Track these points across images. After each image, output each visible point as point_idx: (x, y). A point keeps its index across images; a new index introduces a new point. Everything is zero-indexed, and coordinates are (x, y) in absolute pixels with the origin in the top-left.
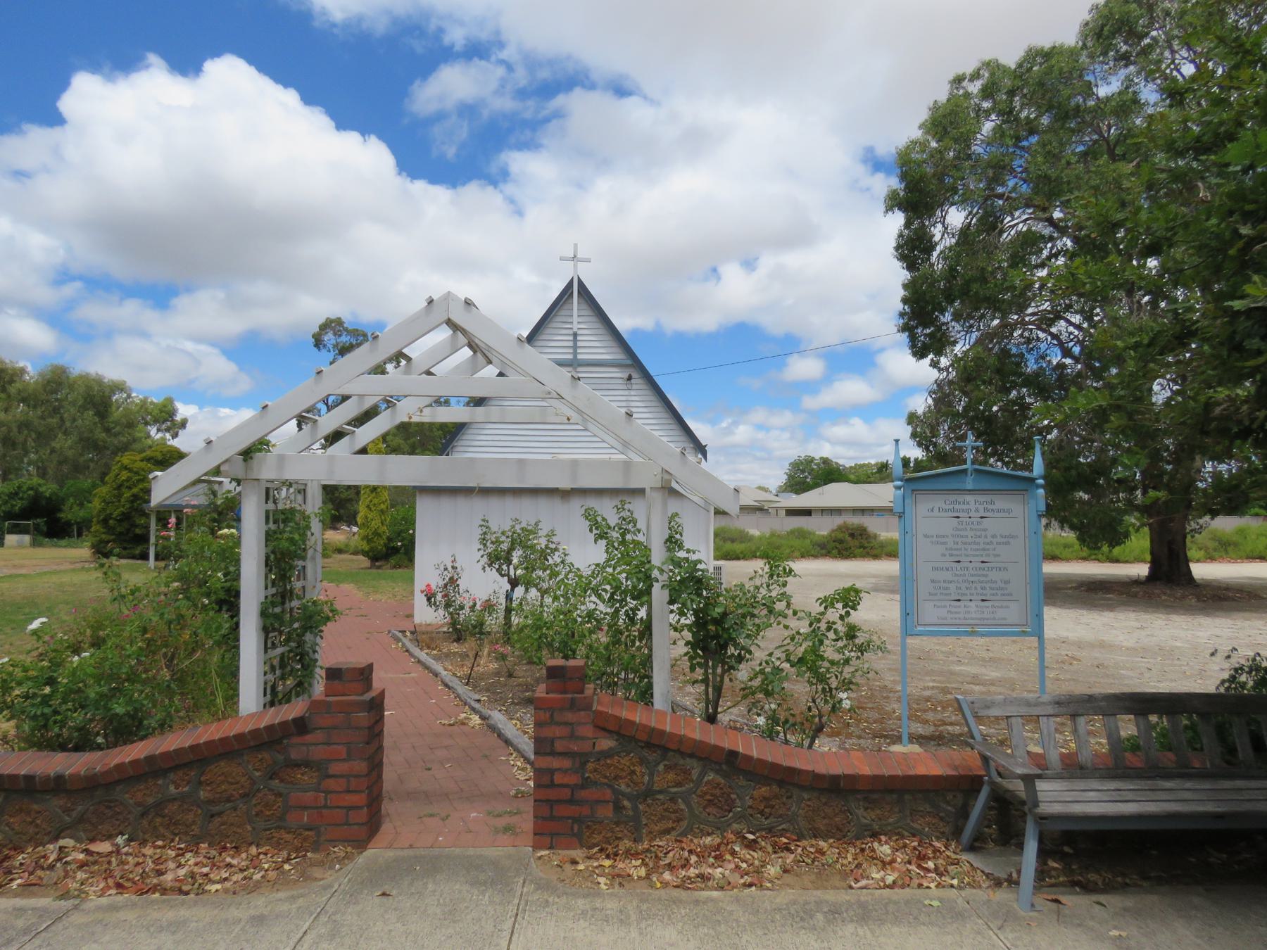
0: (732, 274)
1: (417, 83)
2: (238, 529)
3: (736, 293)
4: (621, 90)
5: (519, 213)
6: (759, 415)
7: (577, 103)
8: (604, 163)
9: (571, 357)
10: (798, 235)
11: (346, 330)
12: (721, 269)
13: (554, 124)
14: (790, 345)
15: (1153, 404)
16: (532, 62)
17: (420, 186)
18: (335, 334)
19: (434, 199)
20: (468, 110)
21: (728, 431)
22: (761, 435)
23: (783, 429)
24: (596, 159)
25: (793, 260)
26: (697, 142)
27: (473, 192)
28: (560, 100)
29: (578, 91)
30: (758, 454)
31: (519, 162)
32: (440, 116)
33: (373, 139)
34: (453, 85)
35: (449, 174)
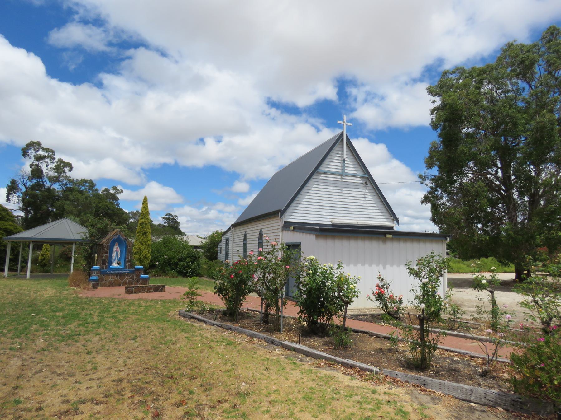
0: (210, 142)
1: (56, 29)
2: (20, 242)
3: (211, 151)
4: (163, 54)
5: (109, 102)
6: (220, 206)
7: (141, 55)
8: (151, 84)
9: (340, 171)
10: (241, 129)
11: (42, 148)
12: (205, 140)
13: (126, 62)
14: (235, 176)
15: (91, 235)
16: (119, 32)
17: (54, 82)
18: (35, 150)
19: (65, 90)
20: (78, 49)
21: (206, 212)
22: (221, 215)
23: (230, 213)
24: (147, 82)
25: (238, 140)
26: (198, 83)
27: (85, 88)
28: (131, 52)
29: (142, 50)
30: (219, 223)
31: (108, 79)
32: (65, 49)
33: (32, 54)
34: (73, 34)
35: (75, 77)
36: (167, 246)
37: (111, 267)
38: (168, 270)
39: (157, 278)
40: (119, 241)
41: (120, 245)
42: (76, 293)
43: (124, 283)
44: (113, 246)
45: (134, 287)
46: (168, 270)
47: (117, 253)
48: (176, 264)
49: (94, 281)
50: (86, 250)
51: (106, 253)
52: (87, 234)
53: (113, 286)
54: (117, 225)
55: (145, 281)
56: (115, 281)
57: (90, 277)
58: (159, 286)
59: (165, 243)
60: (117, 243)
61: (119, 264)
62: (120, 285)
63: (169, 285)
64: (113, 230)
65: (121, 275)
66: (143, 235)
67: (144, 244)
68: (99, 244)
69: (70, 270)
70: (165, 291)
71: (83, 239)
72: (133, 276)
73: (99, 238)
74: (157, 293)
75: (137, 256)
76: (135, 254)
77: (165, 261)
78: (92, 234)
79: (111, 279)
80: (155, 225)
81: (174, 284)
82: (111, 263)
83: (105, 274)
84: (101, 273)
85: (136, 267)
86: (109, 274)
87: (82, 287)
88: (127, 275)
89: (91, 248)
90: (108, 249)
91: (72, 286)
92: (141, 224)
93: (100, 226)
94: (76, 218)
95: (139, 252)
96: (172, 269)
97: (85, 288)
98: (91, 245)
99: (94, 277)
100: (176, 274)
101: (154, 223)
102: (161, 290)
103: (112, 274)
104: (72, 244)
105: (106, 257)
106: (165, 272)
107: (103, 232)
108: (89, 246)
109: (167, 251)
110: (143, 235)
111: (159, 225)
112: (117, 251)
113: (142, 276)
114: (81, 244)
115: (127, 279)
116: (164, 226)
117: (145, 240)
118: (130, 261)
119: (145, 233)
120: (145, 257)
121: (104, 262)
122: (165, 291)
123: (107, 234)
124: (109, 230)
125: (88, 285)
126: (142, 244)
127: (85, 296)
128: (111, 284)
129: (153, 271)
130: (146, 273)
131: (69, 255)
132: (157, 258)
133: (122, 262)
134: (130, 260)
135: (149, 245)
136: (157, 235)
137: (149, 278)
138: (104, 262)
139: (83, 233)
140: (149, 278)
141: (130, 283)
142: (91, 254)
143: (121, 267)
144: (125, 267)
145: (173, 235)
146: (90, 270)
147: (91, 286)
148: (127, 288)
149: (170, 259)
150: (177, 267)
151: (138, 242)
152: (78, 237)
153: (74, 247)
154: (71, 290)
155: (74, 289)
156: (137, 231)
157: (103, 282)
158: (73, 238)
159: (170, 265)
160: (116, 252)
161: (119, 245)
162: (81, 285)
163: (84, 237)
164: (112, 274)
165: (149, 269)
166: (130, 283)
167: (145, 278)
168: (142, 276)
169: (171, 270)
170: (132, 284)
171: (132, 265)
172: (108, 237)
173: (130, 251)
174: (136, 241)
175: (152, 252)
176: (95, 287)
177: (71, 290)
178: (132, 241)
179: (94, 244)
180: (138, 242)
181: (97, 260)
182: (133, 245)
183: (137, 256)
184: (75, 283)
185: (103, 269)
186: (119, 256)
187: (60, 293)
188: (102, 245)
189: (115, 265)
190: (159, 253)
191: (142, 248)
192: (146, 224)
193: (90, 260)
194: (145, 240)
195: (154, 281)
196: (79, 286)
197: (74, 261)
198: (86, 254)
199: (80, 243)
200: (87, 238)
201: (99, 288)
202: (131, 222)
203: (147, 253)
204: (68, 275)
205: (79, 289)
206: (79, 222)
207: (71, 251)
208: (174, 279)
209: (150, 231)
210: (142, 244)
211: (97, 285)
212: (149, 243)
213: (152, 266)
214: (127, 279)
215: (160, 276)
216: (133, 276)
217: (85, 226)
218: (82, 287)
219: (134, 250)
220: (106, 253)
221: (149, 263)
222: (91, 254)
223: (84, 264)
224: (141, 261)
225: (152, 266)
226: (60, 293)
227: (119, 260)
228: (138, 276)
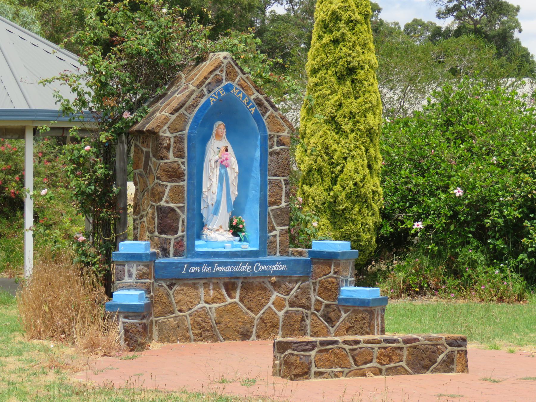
15: (103, 90)
36: (461, 137)
37: (200, 246)
38: (473, 264)
39: (420, 302)
40: (226, 113)
41: (236, 130)
42: (57, 366)
43: (268, 327)
44: (205, 139)
45: (312, 345)
46: (473, 264)
47: (223, 178)
48: (514, 231)
49: (129, 311)
50: (80, 165)
51: (175, 175)
52: (83, 86)
53: (215, 338)
54: (213, 37)
55: (366, 315)
56: (220, 312)
57: (289, 229)
58: (435, 344)
59: (452, 120)
60: (220, 126)
61: (236, 230)
62: (245, 336)
63: (483, 338)
64: (200, 60)
65: (244, 285)
66: (341, 79)
67: (346, 128)
68: (140, 132)
69: (21, 259)
70: (465, 369)
71: (67, 109)
72: (304, 292)
73: (139, 104)
74: (428, 375)
75: (317, 192)
76: (308, 180)
77: (454, 216)
78: (104, 85)
79: (205, 302)
80: (392, 31)
81: (506, 331)
82: (198, 226)
83: (175, 278)
84: (164, 276)
85: (318, 245)
86: (194, 281)
87: (80, 342)
88: (275, 285)
89: (107, 152)
90: (179, 154)
91: (38, 336)
92: (326, 27)
93: (140, 42)
94: (24, 11)
95: (327, 170)
96: (495, 257)
97: (92, 346)
98: (103, 137)
99: (128, 295)
100: (515, 284)
101: (387, 16)
102: (448, 365)
103: (208, 280)
104: (20, 133)
105: (176, 194)
106: (457, 273)
107: (155, 73)
108: (98, 144)
109: (463, 161)
110: (341, 79)
111: (414, 27)
112: (224, 165)
113: (350, 291)
114: (60, 136)
115: (279, 305)
116: (437, 33)
117: (352, 105)
118: (288, 216)
119: (351, 71)
120: (358, 197)
121: (166, 222)
122: (465, 369)
123: (174, 81)
124: (178, 58)
125: (106, 331)
126: (339, 129)
127: (96, 381)
128: (206, 331)
129: (401, 270)
130: (364, 278)
131: (11, 188)
132: (414, 202)
133: (251, 222)
134: (288, 210)
135: (370, 132)
136: (412, 80)
137: (382, 302)
138: (166, 222)
139: (65, 78)
140: (382, 302)
141: (294, 325)
142: (106, 182)
143: (245, 247)
144: (266, 245)
145: (493, 76)
146: (107, 260)
147: (117, 334)
148: (281, 347)
149: (480, 207)
150: (517, 248)
151: (319, 117)
152: (44, 100)
153: (29, 146)
154: (34, 354)
155: (47, 350)
156: (310, 63)
157: (170, 319)
158: (20, 105)
159: (482, 234)
160: (222, 171)
161: (231, 133)
162: (77, 327)
163: (73, 97)
164: (208, 280)
165: (378, 256)
166: (294, 325)
167: (363, 303)
168: (350, 291)
169: (490, 263)
170: (302, 331)
171: (296, 238)
172: (177, 96)
173: (284, 169)
174: (310, 111)
175: (391, 168)
176: (135, 341)
177: (34, 354)
178: (290, 115)
179: (118, 133)
180: (319, 117)
181: (136, 207)
182: (297, 136)
183: (317, 192)
184: (48, 320)
185: (165, 252)
186: (234, 192)
187: (398, 123)
188: (153, 134)
189: (217, 237)
190: (423, 173)
191: (339, 150)
192: (352, 23)
193: (104, 210)
194: (352, 105)
195: (410, 319)
196: (64, 334)
197: (36, 218)
198: (83, 183)
199: (58, 133)
200: (84, 103)
201: (155, 346)
202: (276, 19)
203: (363, 172)
204: (16, 284)
205: (69, 351)
206: (37, 27)
207: (17, 171)
208: (504, 307)
209: (374, 60)
210: (339, 129)
211: (146, 330)
212: (372, 120)
213: (395, 243)
214: (279, 305)
215: (435, 291)
216: (304, 292)
217: (69, 47)
218: (80, 342)
219: (301, 161)
220: (175, 175)
221: (378, 228)
222: (106, 182)
223: (80, 227)
224: (337, 216)
225: (395, 243)
226: (398, 123)
227: (237, 208)
228: (330, 290)
